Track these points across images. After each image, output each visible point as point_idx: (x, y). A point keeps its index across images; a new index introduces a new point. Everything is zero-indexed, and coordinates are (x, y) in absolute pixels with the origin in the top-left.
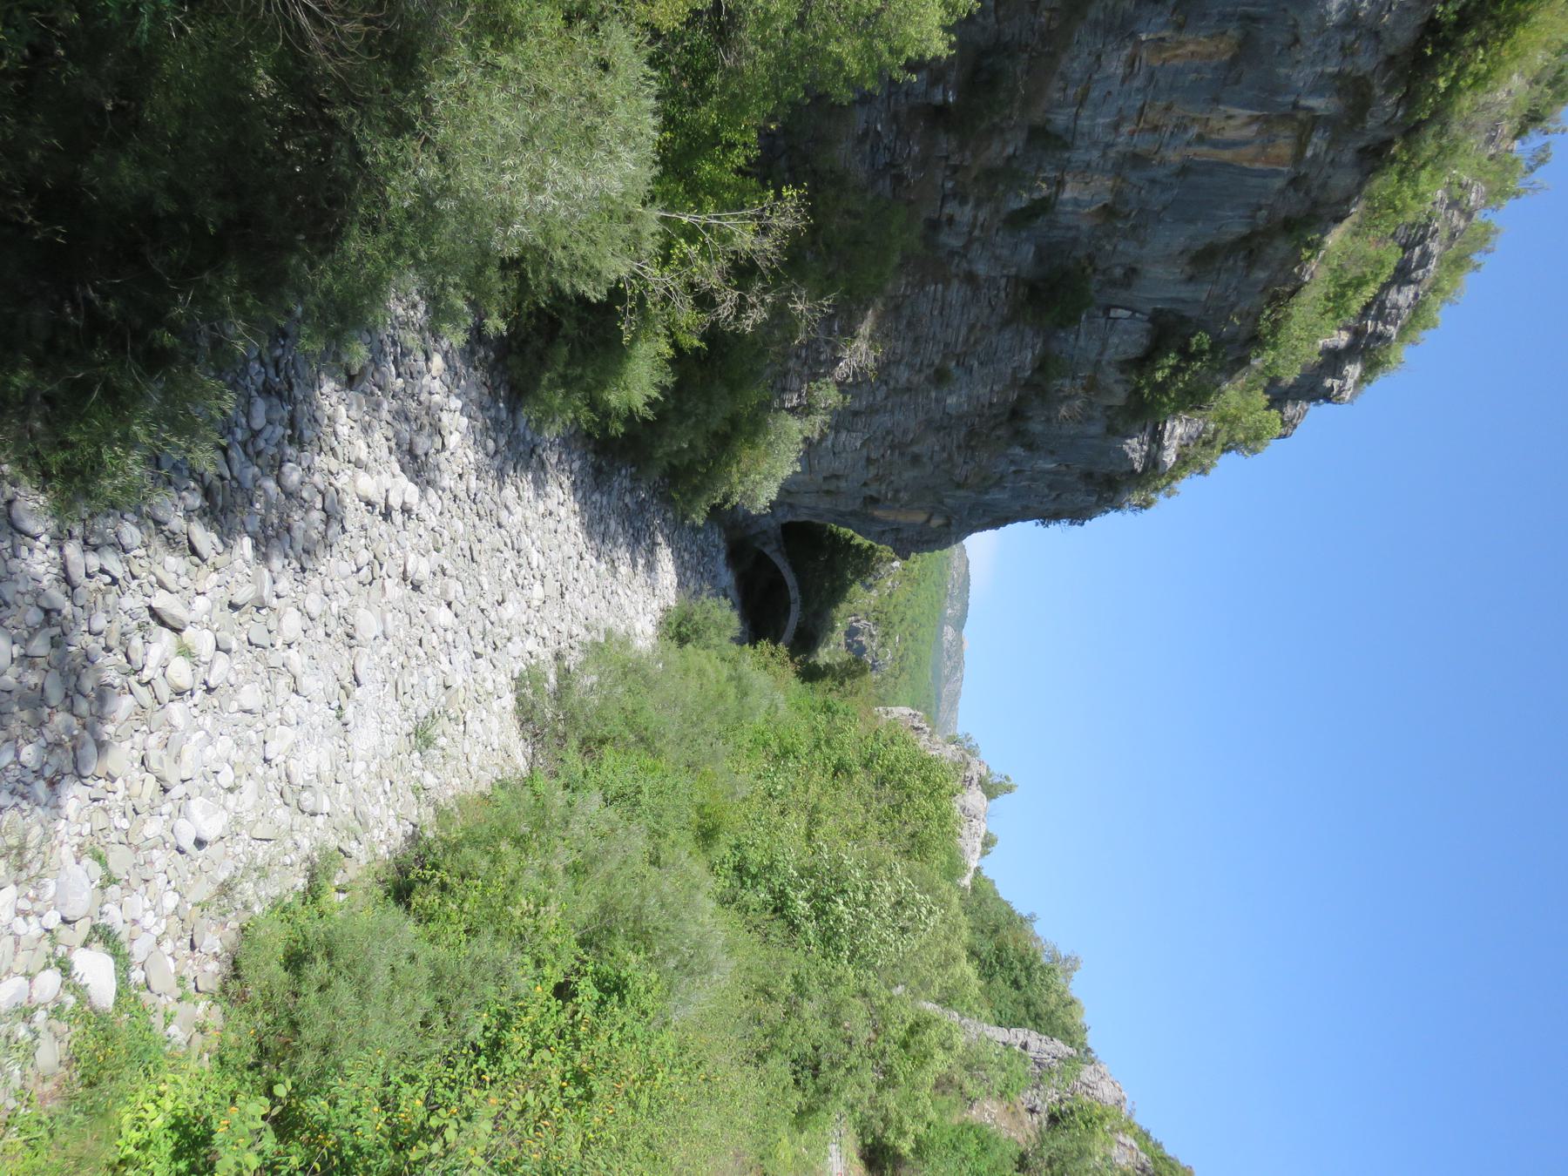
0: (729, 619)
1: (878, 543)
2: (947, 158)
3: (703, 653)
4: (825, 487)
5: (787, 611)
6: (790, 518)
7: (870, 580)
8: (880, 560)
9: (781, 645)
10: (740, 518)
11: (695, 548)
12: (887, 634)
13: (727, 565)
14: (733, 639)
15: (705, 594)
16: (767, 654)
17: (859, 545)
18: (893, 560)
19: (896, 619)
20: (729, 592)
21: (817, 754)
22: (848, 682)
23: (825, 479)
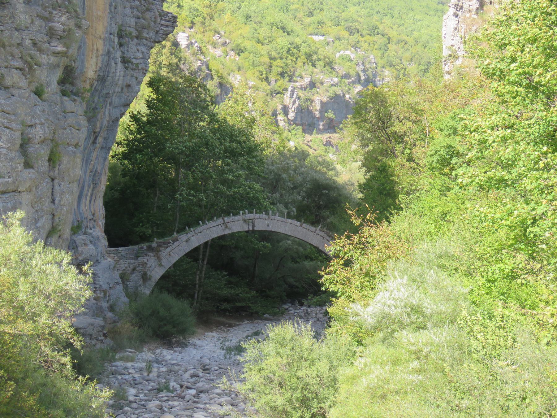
0: (282, 343)
1: (145, 71)
2: (79, 27)
3: (343, 388)
4: (43, 165)
5: (265, 236)
6: (99, 232)
7: (211, 85)
8: (174, 68)
9: (331, 249)
11: (153, 404)
12: (309, 56)
13: (184, 345)
14: (317, 336)
15: (237, 386)
16: (345, 273)
17: (150, 104)
18: (176, 44)
19: (282, 41)
20: (233, 343)
21: (528, 184)
22: (398, 127)
23: (28, 165)
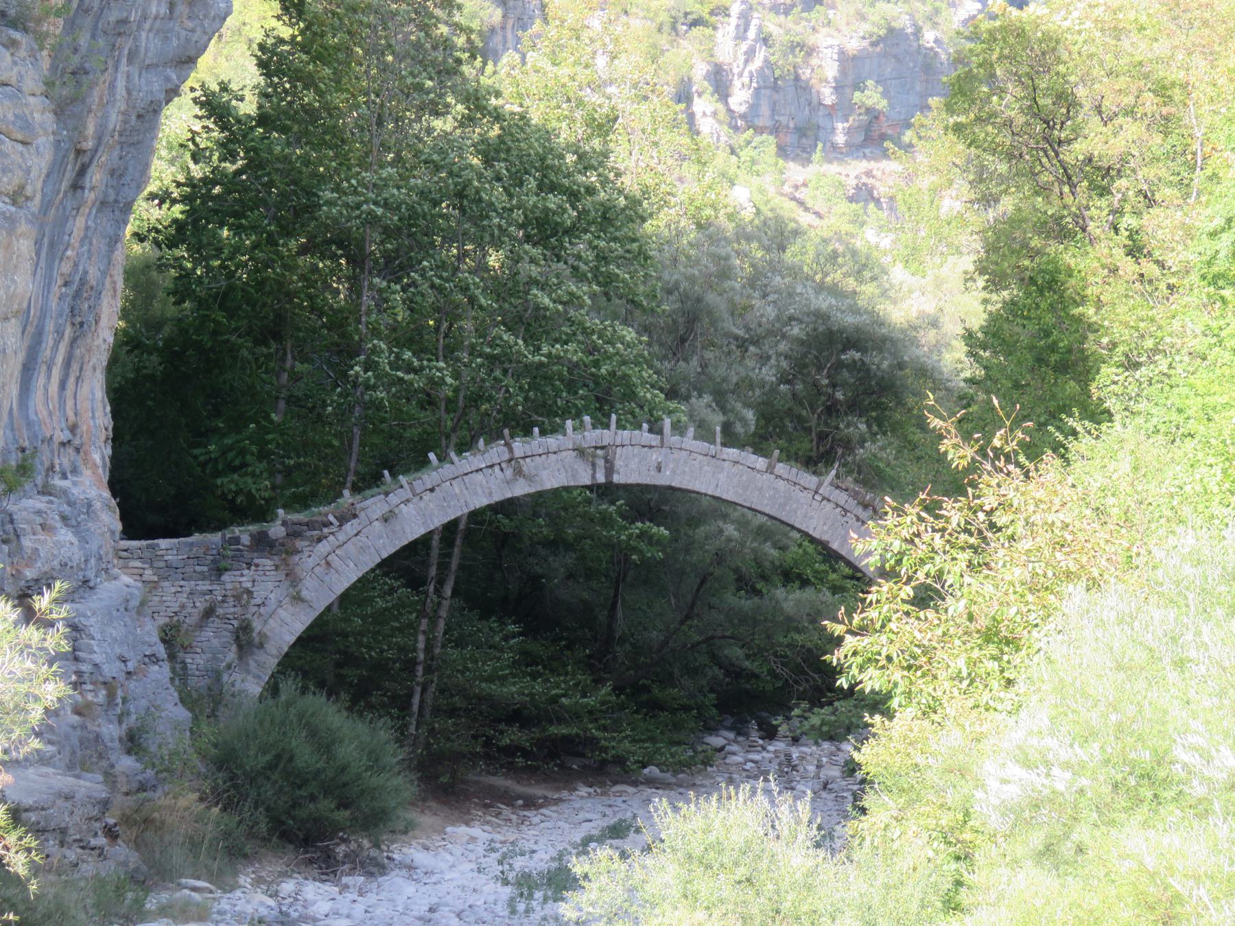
10: (90, 785)
14: (826, 840)
20: (541, 862)
